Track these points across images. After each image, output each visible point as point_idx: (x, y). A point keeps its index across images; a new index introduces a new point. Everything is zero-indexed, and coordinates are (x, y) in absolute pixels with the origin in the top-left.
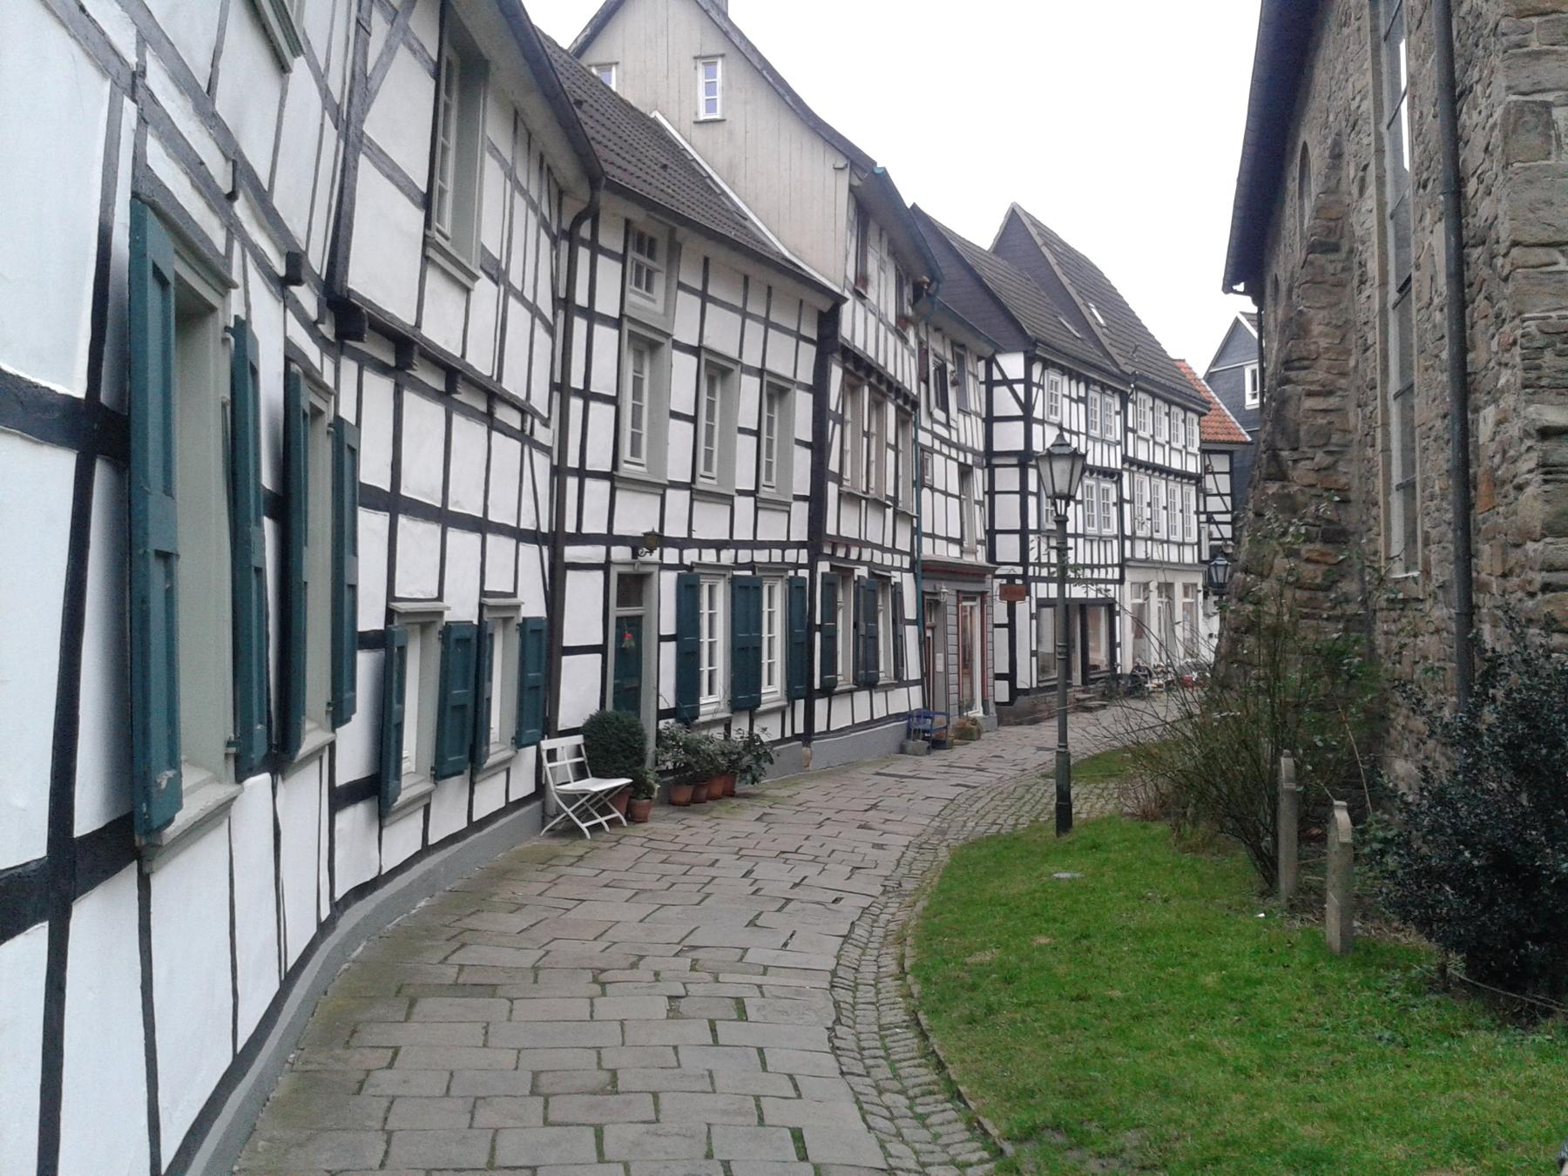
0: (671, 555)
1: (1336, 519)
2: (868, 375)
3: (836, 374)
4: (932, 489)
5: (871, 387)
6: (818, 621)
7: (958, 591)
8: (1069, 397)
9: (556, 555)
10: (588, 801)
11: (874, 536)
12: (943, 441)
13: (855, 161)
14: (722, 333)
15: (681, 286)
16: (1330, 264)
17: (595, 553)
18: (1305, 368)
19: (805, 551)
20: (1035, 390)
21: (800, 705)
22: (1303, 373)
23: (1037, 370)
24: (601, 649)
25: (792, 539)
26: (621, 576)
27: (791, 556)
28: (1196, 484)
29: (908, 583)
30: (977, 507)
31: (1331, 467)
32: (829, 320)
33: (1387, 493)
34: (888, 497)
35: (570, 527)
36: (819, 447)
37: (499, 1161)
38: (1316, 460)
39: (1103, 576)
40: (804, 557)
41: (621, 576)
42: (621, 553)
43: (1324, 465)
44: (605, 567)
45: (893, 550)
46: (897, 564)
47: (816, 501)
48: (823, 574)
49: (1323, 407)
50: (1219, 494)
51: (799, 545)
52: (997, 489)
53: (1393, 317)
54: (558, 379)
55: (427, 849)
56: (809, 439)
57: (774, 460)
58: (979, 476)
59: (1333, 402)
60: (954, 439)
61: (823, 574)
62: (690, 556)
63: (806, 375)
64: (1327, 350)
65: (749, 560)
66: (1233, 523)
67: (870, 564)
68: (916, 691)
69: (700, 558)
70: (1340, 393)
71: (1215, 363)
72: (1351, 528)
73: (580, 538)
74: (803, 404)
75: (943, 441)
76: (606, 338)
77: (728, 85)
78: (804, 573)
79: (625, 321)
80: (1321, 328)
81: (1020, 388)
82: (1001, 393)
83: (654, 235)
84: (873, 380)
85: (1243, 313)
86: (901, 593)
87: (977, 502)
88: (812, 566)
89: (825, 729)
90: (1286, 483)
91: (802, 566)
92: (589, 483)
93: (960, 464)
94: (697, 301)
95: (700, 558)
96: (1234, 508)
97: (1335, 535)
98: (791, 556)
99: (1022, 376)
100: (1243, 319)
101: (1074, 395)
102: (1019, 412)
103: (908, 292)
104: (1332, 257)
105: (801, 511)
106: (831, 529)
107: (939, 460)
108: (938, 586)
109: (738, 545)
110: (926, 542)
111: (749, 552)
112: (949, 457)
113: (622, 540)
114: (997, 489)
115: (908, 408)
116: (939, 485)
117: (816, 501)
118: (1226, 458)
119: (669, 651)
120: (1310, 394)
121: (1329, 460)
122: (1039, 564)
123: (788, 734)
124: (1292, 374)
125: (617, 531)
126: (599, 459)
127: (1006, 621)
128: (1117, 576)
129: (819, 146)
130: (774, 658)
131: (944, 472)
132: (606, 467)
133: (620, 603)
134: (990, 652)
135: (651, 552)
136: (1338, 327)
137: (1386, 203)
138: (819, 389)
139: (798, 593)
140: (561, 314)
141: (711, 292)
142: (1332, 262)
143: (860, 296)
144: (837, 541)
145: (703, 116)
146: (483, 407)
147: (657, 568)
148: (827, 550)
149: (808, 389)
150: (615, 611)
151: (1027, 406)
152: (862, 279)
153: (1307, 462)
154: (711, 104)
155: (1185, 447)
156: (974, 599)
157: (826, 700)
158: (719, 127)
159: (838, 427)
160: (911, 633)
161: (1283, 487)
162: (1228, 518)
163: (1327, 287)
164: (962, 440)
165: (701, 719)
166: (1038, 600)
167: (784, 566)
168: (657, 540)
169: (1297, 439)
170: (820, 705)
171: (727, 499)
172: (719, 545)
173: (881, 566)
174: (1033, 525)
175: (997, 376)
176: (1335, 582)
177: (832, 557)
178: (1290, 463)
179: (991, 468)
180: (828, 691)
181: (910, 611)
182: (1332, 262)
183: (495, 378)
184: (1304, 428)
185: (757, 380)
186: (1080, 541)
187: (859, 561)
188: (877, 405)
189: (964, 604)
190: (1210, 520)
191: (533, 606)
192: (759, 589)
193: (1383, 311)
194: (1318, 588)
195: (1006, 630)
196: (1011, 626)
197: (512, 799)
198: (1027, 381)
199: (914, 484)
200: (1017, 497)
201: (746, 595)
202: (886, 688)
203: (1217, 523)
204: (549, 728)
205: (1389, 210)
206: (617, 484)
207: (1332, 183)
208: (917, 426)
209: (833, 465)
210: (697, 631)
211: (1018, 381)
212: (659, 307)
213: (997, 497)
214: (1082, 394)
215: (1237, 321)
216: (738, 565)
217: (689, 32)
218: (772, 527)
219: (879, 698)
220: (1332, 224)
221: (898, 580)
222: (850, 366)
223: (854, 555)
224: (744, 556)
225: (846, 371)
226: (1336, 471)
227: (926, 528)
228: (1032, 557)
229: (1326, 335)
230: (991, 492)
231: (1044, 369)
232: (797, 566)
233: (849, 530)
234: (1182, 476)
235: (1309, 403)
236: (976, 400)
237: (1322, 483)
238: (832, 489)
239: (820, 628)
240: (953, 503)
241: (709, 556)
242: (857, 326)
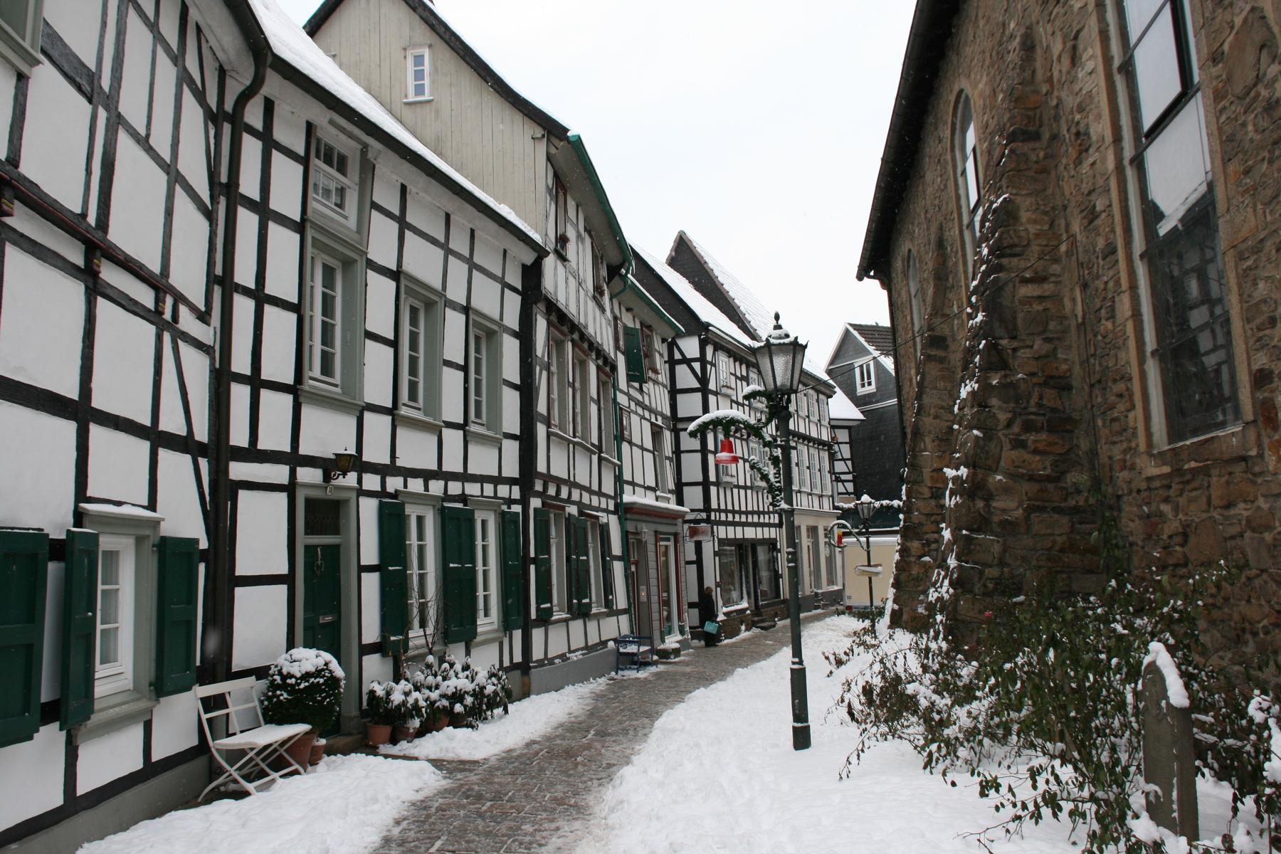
0: (372, 482)
1: (1060, 407)
2: (572, 332)
3: (541, 325)
4: (630, 443)
5: (573, 341)
6: (532, 555)
7: (656, 532)
8: (735, 375)
9: (219, 472)
10: (258, 754)
11: (582, 478)
12: (638, 403)
13: (552, 129)
15: (375, 206)
16: (1035, 152)
17: (279, 473)
18: (1015, 255)
19: (518, 487)
20: (709, 367)
21: (518, 634)
22: (1015, 260)
23: (709, 350)
24: (287, 580)
25: (504, 474)
26: (309, 502)
27: (503, 491)
28: (828, 450)
29: (613, 523)
30: (668, 462)
31: (1052, 355)
32: (532, 274)
33: (1142, 361)
34: (593, 445)
35: (239, 437)
36: (527, 390)
38: (1036, 347)
39: (767, 521)
40: (516, 493)
41: (309, 502)
42: (309, 475)
43: (1043, 353)
44: (290, 489)
45: (600, 493)
46: (603, 506)
48: (535, 509)
49: (1036, 294)
50: (843, 459)
51: (511, 482)
52: (682, 449)
53: (1130, 173)
54: (219, 270)
56: (518, 381)
57: (484, 399)
58: (667, 436)
59: (1048, 288)
60: (647, 403)
61: (535, 509)
62: (394, 483)
63: (512, 320)
64: (1037, 235)
65: (459, 492)
66: (853, 481)
67: (579, 504)
68: (624, 619)
69: (406, 486)
70: (1053, 279)
71: (832, 363)
72: (1076, 416)
73: (253, 454)
74: (510, 348)
75: (638, 403)
76: (284, 244)
77: (435, 70)
78: (517, 508)
79: (308, 225)
80: (1029, 214)
81: (697, 366)
82: (682, 370)
83: (344, 151)
84: (576, 336)
85: (851, 325)
86: (608, 532)
87: (667, 458)
88: (524, 502)
89: (542, 656)
90: (1008, 372)
91: (515, 502)
92: (265, 394)
93: (652, 424)
94: (394, 227)
95: (406, 486)
96: (854, 471)
97: (1061, 424)
99: (698, 355)
100: (851, 329)
101: (738, 374)
102: (696, 385)
103: (604, 273)
104: (1031, 145)
105: (511, 450)
106: (541, 467)
107: (635, 419)
108: (639, 526)
109: (449, 477)
110: (627, 488)
111: (459, 484)
112: (643, 417)
113: (311, 461)
114: (682, 449)
115: (608, 369)
116: (636, 440)
118: (846, 432)
119: (371, 583)
120: (1025, 281)
121: (1047, 347)
122: (719, 510)
123: (506, 663)
124: (1005, 261)
125: (304, 450)
126: (278, 366)
127: (694, 558)
128: (777, 521)
129: (518, 117)
130: (490, 589)
131: (640, 430)
133: (310, 530)
134: (684, 584)
135: (344, 475)
136: (1046, 213)
137: (1112, 57)
138: (525, 335)
139: (508, 525)
140: (223, 201)
141: (409, 219)
142: (1034, 150)
143: (563, 258)
144: (548, 478)
145: (412, 98)
146: (78, 259)
147: (354, 495)
148: (538, 487)
149: (515, 335)
150: (302, 540)
151: (703, 380)
152: (562, 240)
153: (1027, 350)
154: (419, 90)
155: (819, 421)
156: (668, 540)
157: (543, 629)
158: (428, 106)
159: (545, 373)
160: (618, 567)
161: (1006, 376)
162: (850, 477)
163: (1031, 173)
164: (654, 405)
165: (411, 653)
166: (720, 540)
168: (354, 463)
169: (1015, 327)
170: (537, 634)
171: (436, 430)
172: (427, 475)
173: (590, 507)
174: (712, 478)
175: (677, 356)
176: (1064, 473)
177: (542, 495)
178: (1009, 351)
179: (676, 432)
180: (545, 619)
181: (616, 549)
182: (1034, 150)
183: (92, 219)
184: (1020, 316)
185: (463, 317)
186: (749, 492)
187: (569, 500)
188: (581, 365)
189: (662, 543)
190: (838, 480)
192: (471, 521)
193: (1120, 168)
194: (1048, 479)
195: (694, 566)
196: (699, 562)
197: (156, 757)
198: (702, 359)
199: (616, 438)
200: (699, 455)
202: (598, 616)
203: (843, 481)
204: (218, 668)
205: (1117, 63)
206: (302, 399)
207: (1027, 74)
208: (616, 387)
209: (542, 407)
210: (403, 560)
211: (695, 360)
212: (352, 223)
214: (744, 373)
215: (847, 331)
216: (447, 497)
217: (400, 21)
218: (483, 461)
219: (592, 625)
220: (1030, 113)
221: (605, 520)
222: (554, 318)
223: (564, 495)
224: (455, 488)
225: (549, 323)
226: (1055, 356)
227: (627, 476)
228: (714, 505)
229: (1035, 222)
230: (678, 452)
231: (715, 350)
232: (510, 502)
233: (559, 470)
234: (819, 443)
235: (1025, 291)
236: (663, 377)
237: (1043, 371)
238: (541, 430)
239: (534, 561)
240: (649, 457)
241: (416, 485)
242: (555, 279)
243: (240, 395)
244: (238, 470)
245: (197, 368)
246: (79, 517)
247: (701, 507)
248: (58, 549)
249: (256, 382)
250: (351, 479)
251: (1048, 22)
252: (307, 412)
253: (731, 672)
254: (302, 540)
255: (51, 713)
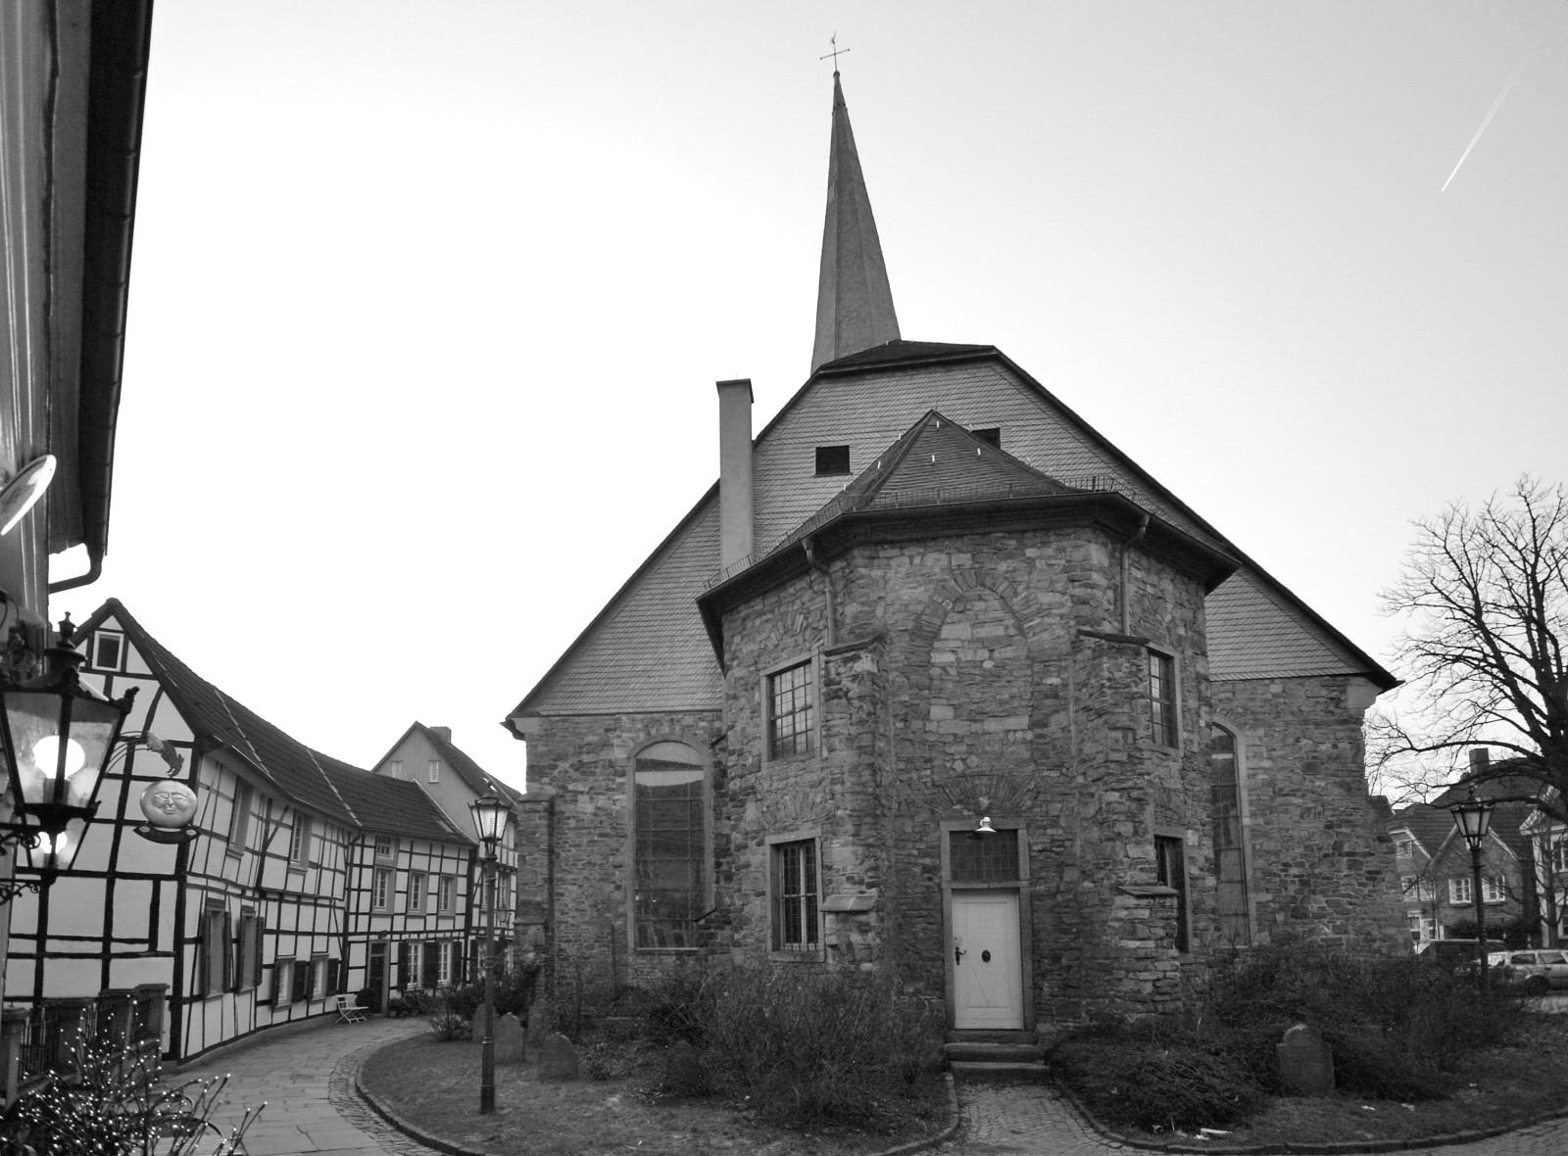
0: (396, 937)
9: (345, 940)
14: (420, 863)
17: (364, 938)
26: (374, 945)
27: (455, 934)
35: (351, 929)
37: (149, 884)
40: (462, 934)
41: (374, 945)
44: (367, 942)
47: (468, 915)
51: (460, 931)
55: (289, 1021)
73: (356, 933)
88: (466, 938)
98: (455, 934)
113: (375, 933)
117: (468, 915)
119: (394, 969)
132: (368, 910)
133: (373, 953)
138: (470, 876)
139: (457, 947)
150: (370, 955)
159: (479, 889)
167: (452, 938)
172: (419, 933)
191: (335, 953)
201: (432, 950)
213: (293, 937)
224: (431, 935)
241: (415, 936)
243: (352, 918)
244: (351, 938)
245: (340, 914)
246: (276, 960)
247: (389, 920)
248: (308, 964)
249: (357, 914)
250: (389, 936)
251: (504, 942)
252: (373, 920)
253: (64, 549)
254: (370, 955)
255: (306, 997)
